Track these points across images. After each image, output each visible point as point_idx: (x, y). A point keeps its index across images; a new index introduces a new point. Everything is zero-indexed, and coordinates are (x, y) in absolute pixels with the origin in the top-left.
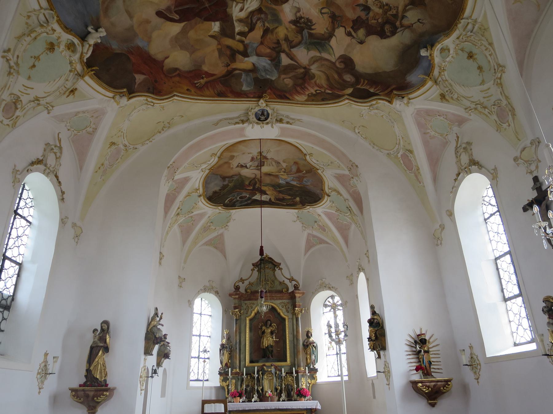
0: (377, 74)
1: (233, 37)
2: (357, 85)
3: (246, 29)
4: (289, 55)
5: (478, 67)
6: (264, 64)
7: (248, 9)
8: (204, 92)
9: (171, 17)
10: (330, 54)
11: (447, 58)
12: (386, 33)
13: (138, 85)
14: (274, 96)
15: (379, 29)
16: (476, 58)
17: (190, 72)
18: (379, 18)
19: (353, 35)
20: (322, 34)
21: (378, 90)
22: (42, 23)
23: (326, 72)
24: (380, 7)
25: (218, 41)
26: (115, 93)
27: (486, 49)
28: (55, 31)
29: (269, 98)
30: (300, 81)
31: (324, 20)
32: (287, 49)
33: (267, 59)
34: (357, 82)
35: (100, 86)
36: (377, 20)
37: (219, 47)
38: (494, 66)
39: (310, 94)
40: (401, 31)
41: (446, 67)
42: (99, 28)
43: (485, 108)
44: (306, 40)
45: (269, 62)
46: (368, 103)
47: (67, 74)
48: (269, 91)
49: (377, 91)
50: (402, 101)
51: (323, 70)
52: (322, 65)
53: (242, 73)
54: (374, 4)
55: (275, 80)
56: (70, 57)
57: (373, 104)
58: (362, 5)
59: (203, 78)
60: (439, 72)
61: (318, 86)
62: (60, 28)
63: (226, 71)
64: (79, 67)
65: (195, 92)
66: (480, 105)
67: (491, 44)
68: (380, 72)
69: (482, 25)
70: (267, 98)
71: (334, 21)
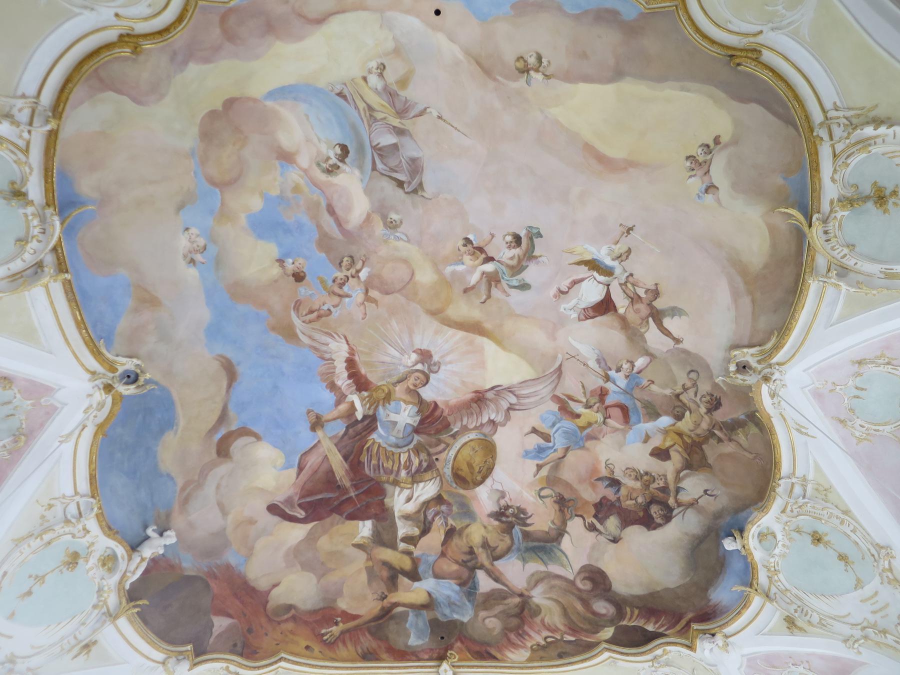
0: (653, 595)
1: (394, 547)
2: (620, 621)
3: (416, 532)
5: (839, 557)
6: (448, 592)
7: (420, 498)
8: (337, 651)
9: (292, 513)
10: (563, 565)
11: (775, 548)
12: (655, 519)
13: (216, 637)
14: (468, 654)
15: (641, 514)
16: (829, 542)
17: (314, 612)
20: (543, 531)
21: (663, 626)
22: (69, 517)
23: (560, 600)
24: (636, 479)
25: (368, 554)
26: (169, 652)
27: (842, 522)
28: (88, 532)
29: (460, 660)
30: (515, 621)
31: (546, 507)
32: (486, 563)
33: (452, 582)
34: (621, 615)
35: (143, 638)
36: (636, 499)
37: (370, 563)
38: (869, 550)
39: (535, 647)
40: (680, 513)
41: (778, 565)
42: (166, 530)
43: (884, 632)
44: (520, 544)
45: (457, 588)
46: (648, 654)
47: (87, 611)
48: (459, 644)
49: (659, 628)
50: (713, 642)
51: (555, 597)
52: (552, 587)
54: (624, 476)
55: (468, 621)
56: (101, 580)
58: (609, 479)
59: (337, 624)
60: (769, 577)
61: (549, 629)
62: (99, 528)
63: (379, 607)
64: (112, 600)
65: (320, 652)
66: (871, 628)
67: (846, 512)
69: (818, 484)
70: (455, 658)
71: (562, 509)
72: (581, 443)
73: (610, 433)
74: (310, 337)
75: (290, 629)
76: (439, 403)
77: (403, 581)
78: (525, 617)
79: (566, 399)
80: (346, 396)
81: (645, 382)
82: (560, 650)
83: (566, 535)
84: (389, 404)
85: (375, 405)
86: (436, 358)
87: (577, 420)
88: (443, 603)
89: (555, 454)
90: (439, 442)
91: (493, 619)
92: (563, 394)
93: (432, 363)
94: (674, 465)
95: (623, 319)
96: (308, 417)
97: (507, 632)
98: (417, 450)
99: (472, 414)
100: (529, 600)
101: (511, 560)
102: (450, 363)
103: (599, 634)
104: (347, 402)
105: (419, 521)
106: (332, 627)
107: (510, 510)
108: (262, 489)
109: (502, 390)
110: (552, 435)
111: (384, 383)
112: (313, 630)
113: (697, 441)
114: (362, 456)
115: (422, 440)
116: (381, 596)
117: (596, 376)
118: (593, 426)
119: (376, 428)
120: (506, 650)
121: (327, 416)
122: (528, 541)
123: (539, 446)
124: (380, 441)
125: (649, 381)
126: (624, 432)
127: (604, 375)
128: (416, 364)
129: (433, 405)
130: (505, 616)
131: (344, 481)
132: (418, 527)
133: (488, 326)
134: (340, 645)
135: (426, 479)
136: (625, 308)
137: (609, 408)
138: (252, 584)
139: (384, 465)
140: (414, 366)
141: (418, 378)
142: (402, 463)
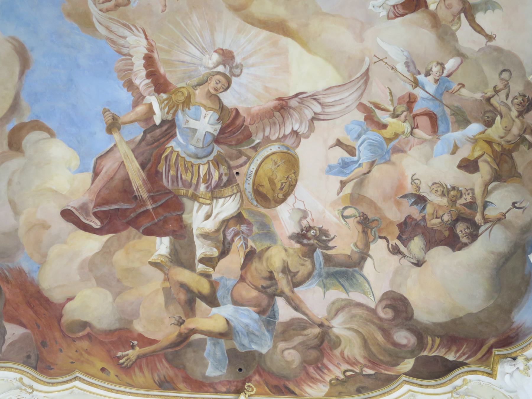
0: (456, 322)
1: (191, 267)
3: (215, 253)
4: (291, 301)
6: (246, 321)
7: (219, 216)
8: (133, 377)
10: (364, 293)
12: (461, 239)
14: (266, 388)
15: (447, 233)
17: (110, 332)
18: (444, 214)
19: (402, 252)
20: (345, 255)
21: (464, 354)
23: (360, 330)
24: (443, 195)
25: (165, 274)
30: (314, 354)
32: (287, 290)
33: (251, 309)
34: (421, 344)
36: (441, 218)
37: (167, 284)
39: (333, 382)
40: (487, 229)
44: (321, 268)
45: (256, 316)
46: (448, 384)
48: (257, 377)
49: (460, 357)
50: (514, 365)
51: (355, 327)
53: (205, 339)
54: (431, 192)
55: (267, 353)
57: (458, 387)
59: (133, 347)
61: (348, 362)
63: (176, 333)
65: (117, 376)
68: (461, 315)
71: (366, 230)
72: (387, 157)
73: (417, 145)
74: (107, 28)
75: (86, 348)
76: (241, 111)
77: (201, 305)
78: (325, 349)
79: (373, 108)
80: (144, 97)
81: (455, 87)
82: (358, 385)
83: (369, 259)
84: (189, 109)
85: (174, 109)
86: (238, 60)
87: (383, 131)
88: (242, 332)
89: (360, 169)
90: (240, 154)
91: (292, 351)
92: (369, 102)
93: (234, 65)
94: (482, 177)
95: (434, 17)
96: (104, 117)
97: (306, 365)
98: (218, 162)
99: (275, 123)
100: (330, 331)
101: (312, 287)
102: (253, 65)
103: (398, 367)
104: (145, 104)
105: (218, 241)
106: (128, 350)
107: (312, 231)
108: (56, 191)
109: (307, 97)
110: (357, 147)
111: (183, 85)
112: (109, 351)
113: (507, 148)
114: (160, 166)
115: (222, 151)
116: (179, 321)
117: (403, 80)
118: (400, 137)
119: (174, 136)
120: (305, 385)
121: (124, 118)
122: (329, 266)
123: (343, 161)
124: (178, 149)
125: (459, 84)
126: (432, 143)
127: (412, 79)
128: (217, 66)
129: (234, 113)
130: (304, 347)
131: (141, 192)
132: (217, 248)
133: (293, 25)
134: (137, 370)
135: (226, 195)
136: (436, 4)
137: (417, 118)
138: (46, 294)
139: (183, 177)
140: (215, 67)
141: (220, 82)
142: (202, 176)
